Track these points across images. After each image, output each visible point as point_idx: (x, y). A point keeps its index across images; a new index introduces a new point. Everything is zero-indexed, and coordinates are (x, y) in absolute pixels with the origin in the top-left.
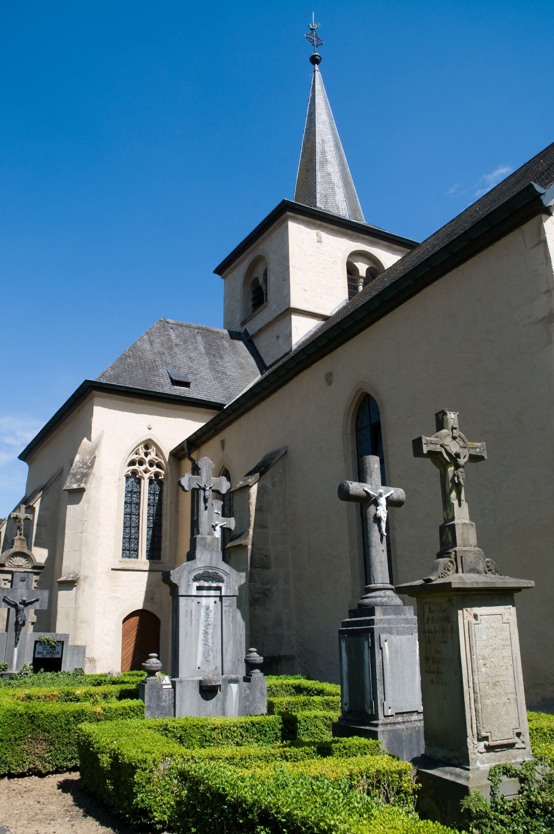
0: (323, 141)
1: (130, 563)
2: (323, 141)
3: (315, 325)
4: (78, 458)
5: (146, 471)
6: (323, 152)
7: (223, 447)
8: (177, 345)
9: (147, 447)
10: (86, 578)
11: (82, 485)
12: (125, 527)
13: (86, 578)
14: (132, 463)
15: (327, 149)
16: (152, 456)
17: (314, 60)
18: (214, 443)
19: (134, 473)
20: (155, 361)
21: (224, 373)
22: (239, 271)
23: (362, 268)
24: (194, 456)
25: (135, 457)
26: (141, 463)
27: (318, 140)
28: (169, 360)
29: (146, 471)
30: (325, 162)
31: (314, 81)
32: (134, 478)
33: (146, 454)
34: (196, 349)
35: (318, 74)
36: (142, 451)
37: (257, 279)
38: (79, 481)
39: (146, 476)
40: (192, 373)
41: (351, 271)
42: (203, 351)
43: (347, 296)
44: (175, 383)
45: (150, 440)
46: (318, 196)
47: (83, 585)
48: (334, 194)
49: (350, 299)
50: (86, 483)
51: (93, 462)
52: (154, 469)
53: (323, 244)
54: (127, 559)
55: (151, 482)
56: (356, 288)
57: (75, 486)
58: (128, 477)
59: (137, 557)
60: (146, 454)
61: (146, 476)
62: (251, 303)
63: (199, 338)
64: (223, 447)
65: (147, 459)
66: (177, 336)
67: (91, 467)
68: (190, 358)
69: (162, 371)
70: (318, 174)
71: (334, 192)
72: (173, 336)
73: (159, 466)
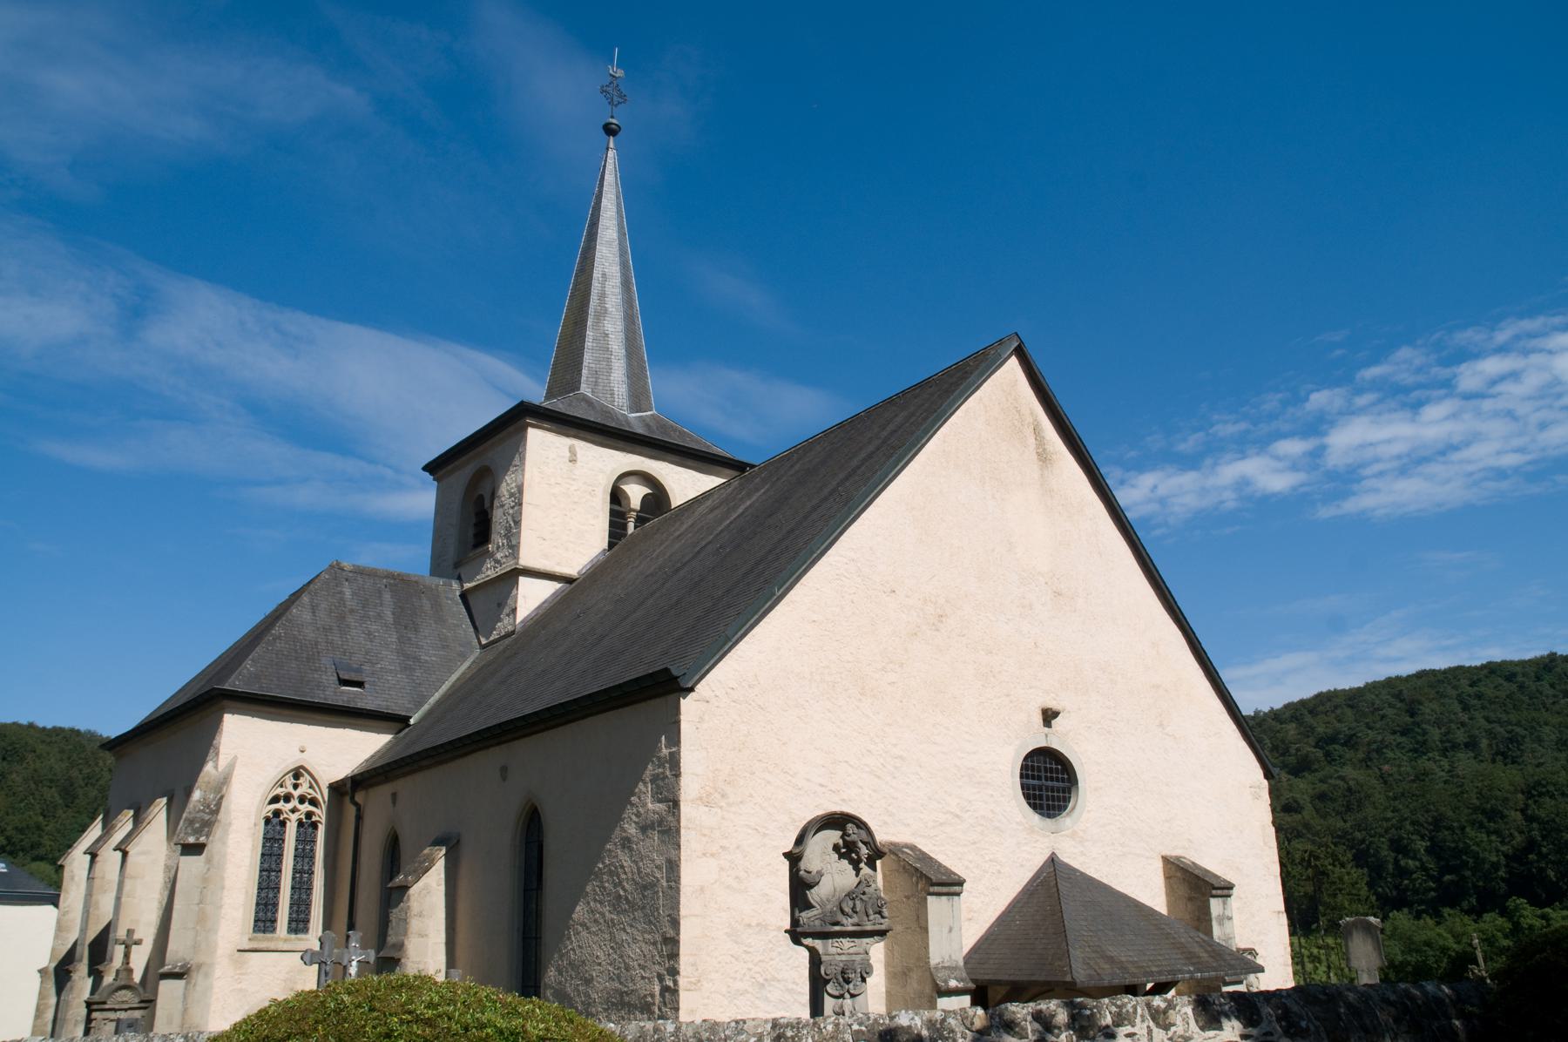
0: (604, 275)
1: (264, 941)
2: (604, 275)
3: (552, 591)
4: (197, 795)
5: (293, 811)
6: (602, 296)
7: (394, 803)
8: (352, 611)
9: (297, 775)
10: (199, 966)
11: (202, 839)
12: (260, 889)
13: (199, 966)
14: (275, 800)
15: (608, 290)
16: (304, 789)
17: (610, 130)
18: (384, 791)
19: (277, 813)
20: (317, 643)
21: (417, 659)
22: (461, 476)
23: (636, 493)
24: (359, 798)
25: (280, 791)
26: (287, 798)
27: (597, 274)
28: (337, 640)
29: (293, 811)
30: (602, 313)
31: (601, 185)
32: (274, 824)
33: (296, 786)
34: (379, 616)
35: (611, 154)
36: (289, 781)
37: (481, 497)
38: (198, 832)
39: (294, 817)
40: (369, 661)
41: (617, 496)
42: (389, 617)
43: (606, 545)
44: (345, 682)
45: (302, 767)
46: (584, 372)
47: (198, 978)
48: (610, 369)
49: (611, 545)
50: (208, 836)
51: (219, 805)
52: (306, 807)
53: (579, 464)
54: (260, 935)
55: (300, 824)
56: (625, 527)
57: (191, 840)
58: (267, 821)
59: (274, 930)
60: (296, 786)
61: (294, 817)
62: (471, 532)
63: (387, 596)
64: (394, 803)
65: (296, 793)
66: (354, 594)
67: (217, 811)
68: (370, 633)
69: (326, 661)
70: (589, 333)
71: (608, 379)
72: (348, 593)
73: (314, 802)
